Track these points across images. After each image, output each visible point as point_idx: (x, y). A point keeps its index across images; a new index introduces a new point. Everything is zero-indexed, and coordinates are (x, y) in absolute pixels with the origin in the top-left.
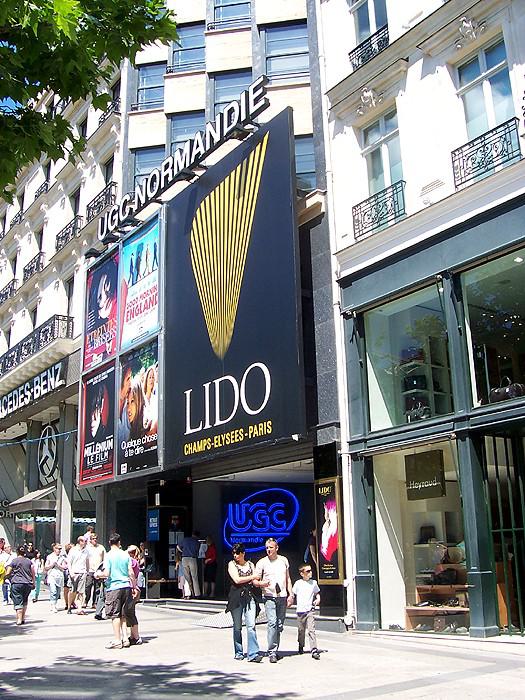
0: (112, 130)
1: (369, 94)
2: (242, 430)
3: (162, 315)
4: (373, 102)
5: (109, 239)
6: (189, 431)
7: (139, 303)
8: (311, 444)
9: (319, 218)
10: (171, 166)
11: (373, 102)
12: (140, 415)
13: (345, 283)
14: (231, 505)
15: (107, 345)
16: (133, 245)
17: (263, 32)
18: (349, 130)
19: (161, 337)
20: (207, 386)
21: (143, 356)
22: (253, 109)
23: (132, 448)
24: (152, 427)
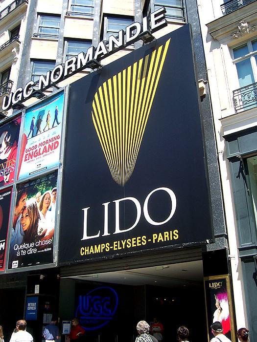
0: (13, 51)
1: (246, 25)
2: (108, 244)
3: (62, 155)
4: (248, 30)
5: (19, 105)
6: (85, 237)
7: (38, 149)
8: (200, 250)
9: (205, 98)
10: (74, 62)
11: (248, 30)
12: (34, 225)
13: (229, 138)
14: (81, 297)
15: (5, 177)
16: (35, 113)
17: (32, 62)
18: (225, 48)
19: (61, 171)
20: (106, 205)
21: (39, 184)
22: (153, 26)
23: (24, 249)
24: (47, 234)
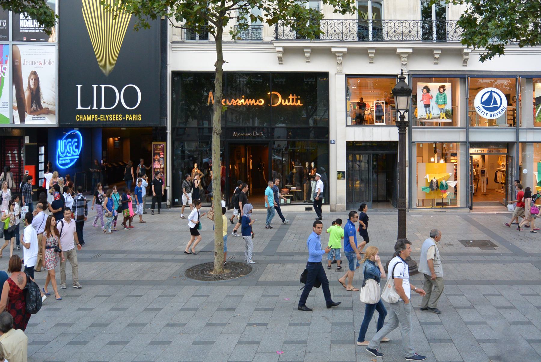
6: (79, 108)
20: (95, 87)
